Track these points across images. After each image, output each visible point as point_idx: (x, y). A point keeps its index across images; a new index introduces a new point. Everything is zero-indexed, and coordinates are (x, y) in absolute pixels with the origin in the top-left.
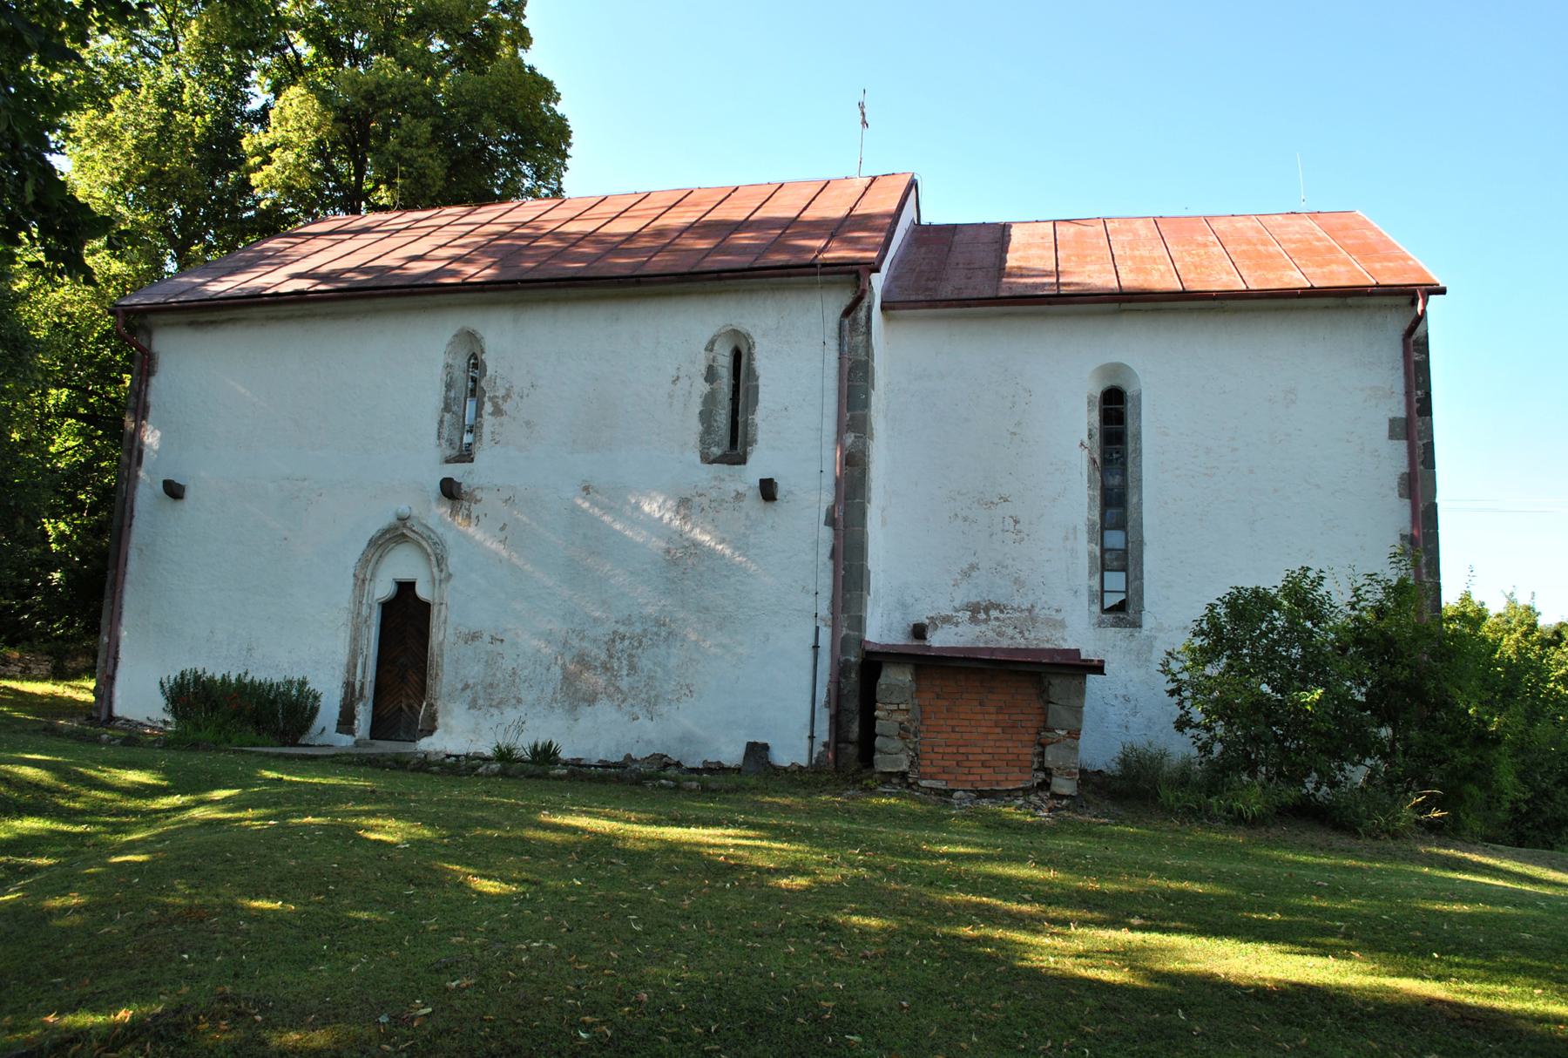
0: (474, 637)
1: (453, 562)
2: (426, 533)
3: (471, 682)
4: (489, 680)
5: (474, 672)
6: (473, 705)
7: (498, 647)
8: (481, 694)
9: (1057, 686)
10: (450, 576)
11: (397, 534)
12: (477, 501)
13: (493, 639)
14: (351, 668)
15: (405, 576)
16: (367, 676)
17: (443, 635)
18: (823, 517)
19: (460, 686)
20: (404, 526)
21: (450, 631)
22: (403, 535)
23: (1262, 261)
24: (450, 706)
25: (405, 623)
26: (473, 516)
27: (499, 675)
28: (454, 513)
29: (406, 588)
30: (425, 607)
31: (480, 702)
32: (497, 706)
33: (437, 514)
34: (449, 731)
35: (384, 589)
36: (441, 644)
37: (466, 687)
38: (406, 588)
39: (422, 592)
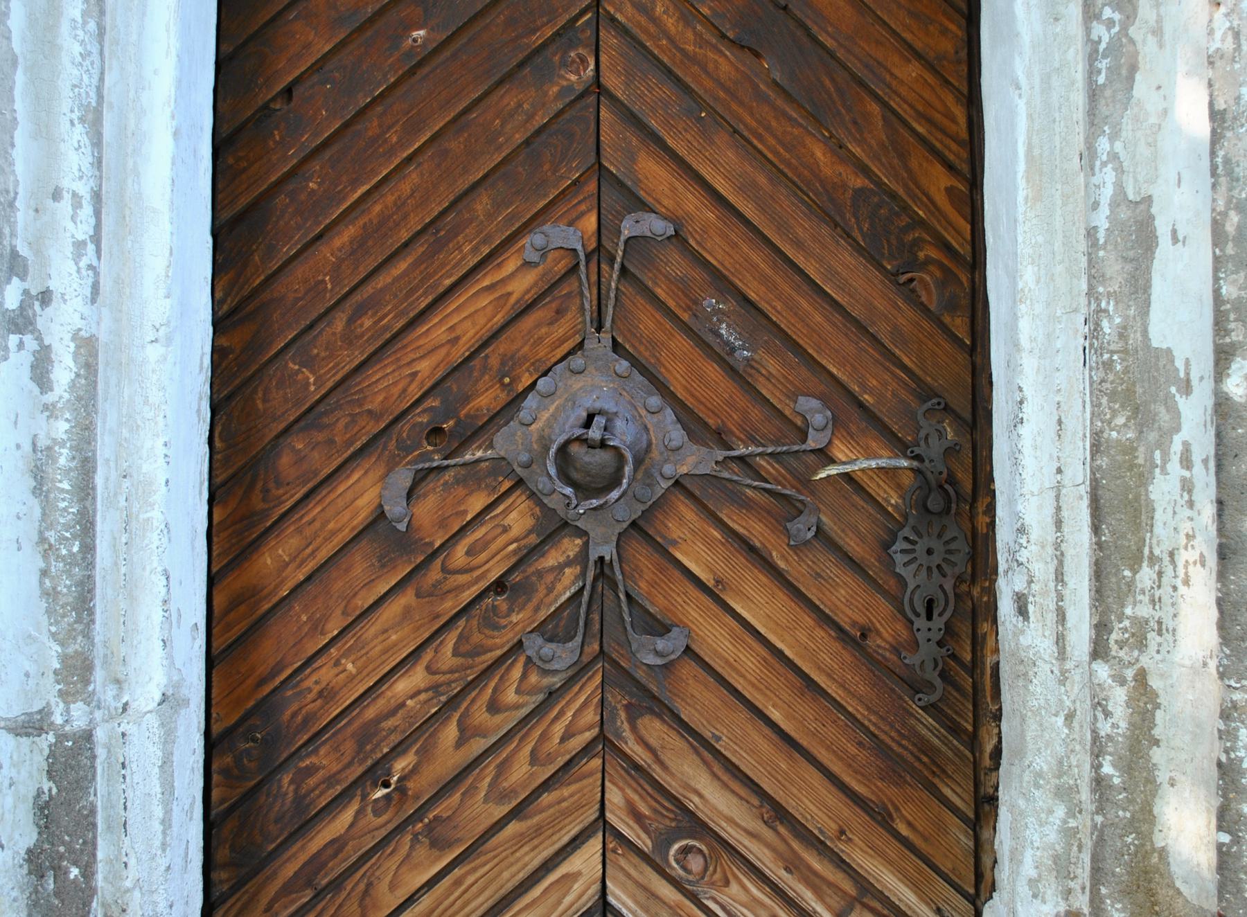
9: (752, 623)
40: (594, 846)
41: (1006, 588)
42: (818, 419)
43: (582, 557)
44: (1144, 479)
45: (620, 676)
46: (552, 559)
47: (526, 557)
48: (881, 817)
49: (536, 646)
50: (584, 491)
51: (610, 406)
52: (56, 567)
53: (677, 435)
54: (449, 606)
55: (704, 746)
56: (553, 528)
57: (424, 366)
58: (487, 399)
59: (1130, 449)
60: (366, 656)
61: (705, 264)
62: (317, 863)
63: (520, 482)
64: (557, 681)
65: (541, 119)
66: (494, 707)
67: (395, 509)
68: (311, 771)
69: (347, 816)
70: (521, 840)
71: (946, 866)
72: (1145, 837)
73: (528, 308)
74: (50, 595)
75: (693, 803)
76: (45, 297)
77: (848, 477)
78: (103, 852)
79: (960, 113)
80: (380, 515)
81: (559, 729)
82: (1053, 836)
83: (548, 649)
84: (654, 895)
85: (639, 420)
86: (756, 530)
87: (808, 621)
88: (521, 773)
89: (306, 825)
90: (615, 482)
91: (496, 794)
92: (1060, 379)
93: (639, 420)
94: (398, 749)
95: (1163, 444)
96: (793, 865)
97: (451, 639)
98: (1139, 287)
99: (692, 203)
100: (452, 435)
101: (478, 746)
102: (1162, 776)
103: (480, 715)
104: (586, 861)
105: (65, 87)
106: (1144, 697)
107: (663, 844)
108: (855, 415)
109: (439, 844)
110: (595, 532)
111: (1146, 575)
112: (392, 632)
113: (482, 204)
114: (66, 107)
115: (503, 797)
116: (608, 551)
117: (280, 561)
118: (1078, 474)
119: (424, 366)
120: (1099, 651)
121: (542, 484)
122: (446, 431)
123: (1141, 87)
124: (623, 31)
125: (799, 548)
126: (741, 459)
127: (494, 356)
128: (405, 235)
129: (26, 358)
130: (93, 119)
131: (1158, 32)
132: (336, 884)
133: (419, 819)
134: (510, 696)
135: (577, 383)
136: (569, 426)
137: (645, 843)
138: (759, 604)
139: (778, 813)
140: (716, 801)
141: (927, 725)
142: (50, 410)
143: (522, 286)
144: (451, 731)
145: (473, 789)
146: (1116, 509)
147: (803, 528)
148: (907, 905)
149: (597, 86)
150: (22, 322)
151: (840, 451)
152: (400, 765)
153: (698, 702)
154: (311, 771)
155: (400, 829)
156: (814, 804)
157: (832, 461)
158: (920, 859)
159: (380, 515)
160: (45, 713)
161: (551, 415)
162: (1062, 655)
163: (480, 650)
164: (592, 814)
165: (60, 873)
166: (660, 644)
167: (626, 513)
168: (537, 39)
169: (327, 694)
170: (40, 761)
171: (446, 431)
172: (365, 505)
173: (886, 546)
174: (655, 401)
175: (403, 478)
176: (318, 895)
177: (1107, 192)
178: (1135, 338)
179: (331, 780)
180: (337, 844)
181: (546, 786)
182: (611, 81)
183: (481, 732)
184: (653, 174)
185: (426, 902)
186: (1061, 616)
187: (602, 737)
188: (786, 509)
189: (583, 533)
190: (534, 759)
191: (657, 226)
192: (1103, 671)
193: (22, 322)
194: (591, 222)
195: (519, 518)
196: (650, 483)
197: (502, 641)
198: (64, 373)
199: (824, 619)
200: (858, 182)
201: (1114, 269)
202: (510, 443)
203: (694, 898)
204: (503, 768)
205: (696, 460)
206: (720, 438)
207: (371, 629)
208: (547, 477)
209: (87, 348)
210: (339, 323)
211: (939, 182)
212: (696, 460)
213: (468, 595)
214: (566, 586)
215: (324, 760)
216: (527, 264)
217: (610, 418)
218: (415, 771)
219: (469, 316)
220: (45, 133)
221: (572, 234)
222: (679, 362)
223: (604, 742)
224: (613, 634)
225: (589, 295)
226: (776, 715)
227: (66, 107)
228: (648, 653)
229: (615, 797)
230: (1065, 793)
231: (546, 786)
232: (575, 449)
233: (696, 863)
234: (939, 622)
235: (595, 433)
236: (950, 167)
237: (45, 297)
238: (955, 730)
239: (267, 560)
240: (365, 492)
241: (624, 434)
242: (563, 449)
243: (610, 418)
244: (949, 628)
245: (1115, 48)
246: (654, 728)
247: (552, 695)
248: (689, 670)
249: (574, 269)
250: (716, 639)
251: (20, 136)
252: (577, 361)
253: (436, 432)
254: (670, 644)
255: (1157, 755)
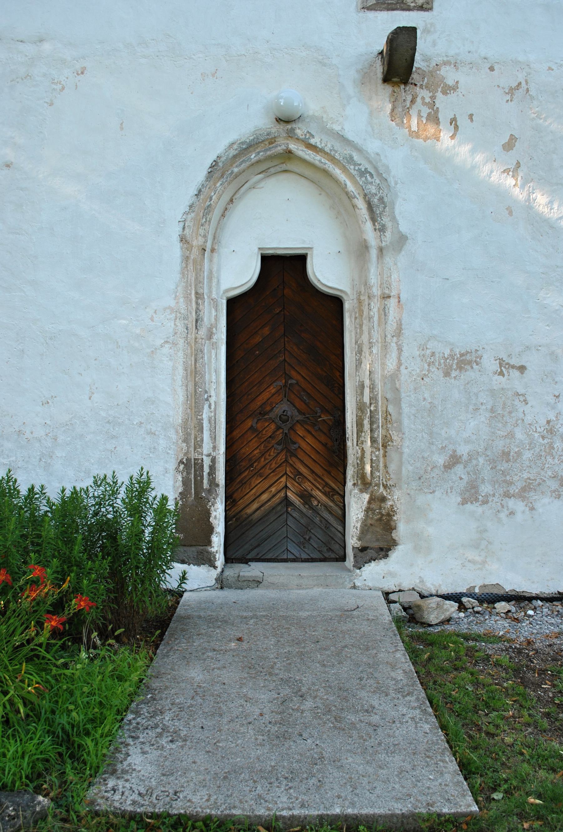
0: (464, 361)
1: (407, 210)
2: (341, 151)
3: (463, 450)
4: (500, 445)
5: (468, 430)
6: (471, 495)
7: (515, 381)
8: (486, 473)
9: (307, 442)
10: (402, 239)
11: (277, 150)
12: (448, 90)
13: (504, 367)
14: (192, 431)
15: (285, 243)
16: (214, 447)
17: (370, 363)
18: (347, 306)
19: (441, 460)
20: (291, 135)
21: (411, 350)
22: (289, 154)
23: (304, 242)
24: (421, 500)
25: (285, 333)
26: (444, 116)
27: (519, 435)
28: (399, 113)
29: (283, 270)
30: (335, 303)
31: (485, 489)
32: (523, 494)
33: (359, 118)
34: (422, 545)
35: (239, 273)
36: (394, 377)
37: (454, 460)
38: (283, 270)
39: (326, 273)
40: (285, 477)
41: (347, 436)
42: (319, 411)
43: (283, 432)
44: (363, 420)
45: (289, 451)
46: (278, 433)
47: (274, 432)
48: (329, 473)
49: (276, 446)
50: (283, 422)
51: (287, 409)
52: (212, 433)
53: (297, 414)
54: (262, 440)
55: (302, 462)
56: (278, 428)
57: (258, 403)
58: (268, 408)
59: (361, 416)
60: (252, 448)
61: (301, 387)
62: (243, 479)
63: (273, 421)
64: (279, 451)
65: (276, 365)
66: (269, 455)
67: (254, 425)
68: (241, 465)
69: (247, 472)
70: (274, 476)
71: (339, 480)
72: (363, 471)
73: (274, 395)
74: (211, 437)
75: (300, 470)
76: (210, 396)
77: (323, 420)
78: (217, 474)
79: (341, 363)
80: (252, 426)
81: (279, 459)
82: (352, 472)
83: (278, 446)
84: (293, 484)
85: (291, 411)
86: (309, 428)
87: (317, 442)
88: (274, 466)
89: (240, 474)
90: (288, 421)
91: (270, 469)
92: (352, 406)
93: (291, 411)
94: (255, 462)
95: (366, 416)
96: (315, 480)
97: (263, 445)
98: (362, 393)
99: (299, 378)
100: (262, 413)
101: (267, 461)
102: (366, 462)
103: (267, 457)
104: (283, 479)
105: (212, 367)
106: (363, 451)
107: (295, 476)
108: (324, 410)
109: (261, 476)
110: (285, 429)
111: (363, 434)
112: (254, 444)
113: (267, 379)
114: (213, 370)
115: (271, 469)
116: (287, 431)
117: (237, 433)
118: (355, 420)
119: (258, 403)
120: (357, 445)
121: (277, 421)
122: (262, 413)
123: (363, 365)
124: (288, 351)
125: (316, 431)
126: (307, 417)
127: (269, 401)
128: (256, 383)
129: (208, 405)
130: (216, 372)
131: (365, 357)
132: (245, 483)
133: (258, 474)
134: (272, 454)
135: (282, 406)
136: (281, 412)
137: (292, 476)
138: (309, 439)
139: (313, 472)
140: (303, 470)
141: (336, 459)
142: (211, 412)
143: (273, 391)
144: (263, 459)
145: (266, 468)
146: (360, 424)
147: (316, 428)
148: (211, 272)
149: (285, 360)
150: (207, 400)
151: (322, 416)
152: (255, 464)
153: (301, 455)
154: (241, 465)
155: (255, 474)
156: (318, 470)
157: (321, 417)
158: (335, 479)
159: (252, 426)
160: (210, 453)
161: (278, 411)
162: (353, 446)
163: (267, 447)
164: (284, 472)
165: (212, 476)
166: (295, 446)
167: (289, 426)
168: (275, 353)
169: (244, 454)
170: (210, 460)
171: (262, 413)
172: (250, 424)
173: (330, 430)
174: (294, 408)
175: (256, 420)
176: (243, 484)
177: (358, 380)
178: (361, 401)
179: (244, 467)
180: (245, 477)
181: (277, 468)
182: (287, 359)
183: (267, 459)
184: (293, 374)
185: (259, 486)
186: (353, 440)
187: (286, 460)
188: (314, 425)
189: (283, 429)
190: (276, 463)
191: (294, 382)
192: (358, 448)
193: (207, 400)
194: (284, 381)
195: (273, 427)
196: (293, 421)
197: (271, 445)
198: (213, 407)
199: (319, 441)
200: (325, 374)
201: (359, 391)
202: (272, 415)
203: (300, 485)
204: (271, 464)
205: (300, 417)
206: (304, 414)
207: (250, 444)
208: (278, 420)
209: (215, 402)
210: (246, 397)
211: (338, 374)
212: (300, 417)
213: (265, 438)
214: (280, 437)
215: (243, 464)
216: (274, 388)
217: (287, 411)
218: (257, 465)
219: (265, 396)
220: (210, 374)
221: (281, 383)
222: (297, 402)
223: (286, 461)
224: (288, 445)
225: (284, 392)
226: (313, 457)
227: (213, 370)
228: (293, 447)
229: (288, 469)
230: (353, 466)
231: (277, 468)
232: (282, 416)
233: (300, 480)
234: (338, 442)
235: (285, 414)
236: (339, 372)
237: (210, 396)
238: (341, 459)
239: (234, 433)
240: (249, 423)
241: (289, 413)
242: (280, 416)
243: (287, 411)
244: (339, 443)
245: (359, 360)
246: (294, 459)
247: (278, 454)
248: (299, 450)
249: (281, 388)
250: (303, 445)
251: (206, 374)
252: (282, 402)
253: (260, 413)
254: (296, 446)
255: (365, 459)
